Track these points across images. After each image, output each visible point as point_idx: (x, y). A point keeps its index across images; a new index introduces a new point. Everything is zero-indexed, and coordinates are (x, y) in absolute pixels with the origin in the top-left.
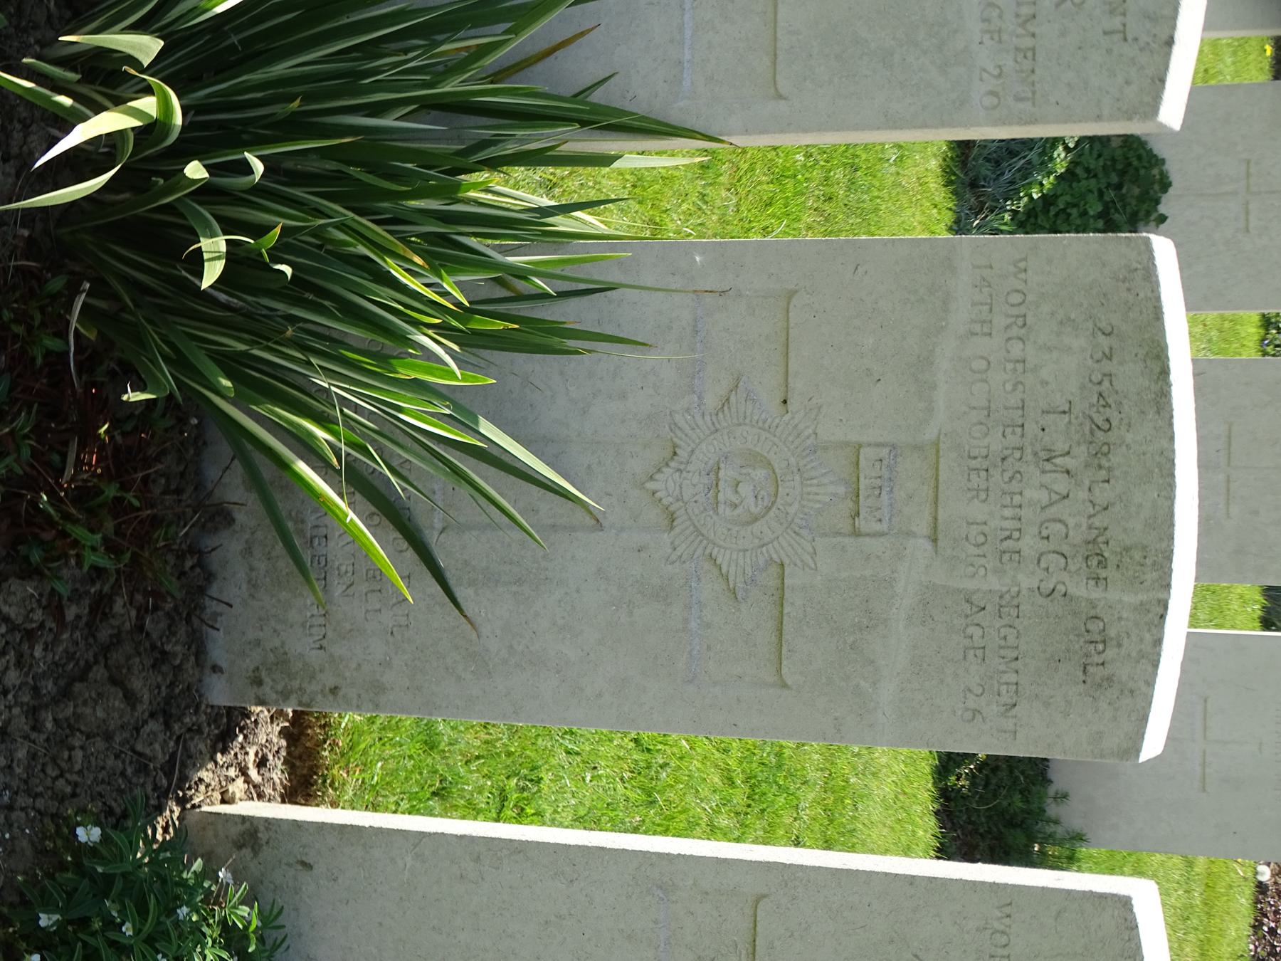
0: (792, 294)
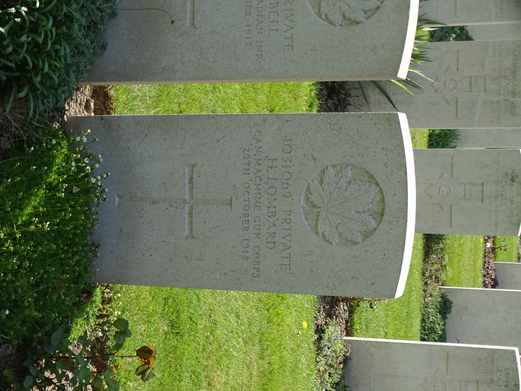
0: (459, 51)
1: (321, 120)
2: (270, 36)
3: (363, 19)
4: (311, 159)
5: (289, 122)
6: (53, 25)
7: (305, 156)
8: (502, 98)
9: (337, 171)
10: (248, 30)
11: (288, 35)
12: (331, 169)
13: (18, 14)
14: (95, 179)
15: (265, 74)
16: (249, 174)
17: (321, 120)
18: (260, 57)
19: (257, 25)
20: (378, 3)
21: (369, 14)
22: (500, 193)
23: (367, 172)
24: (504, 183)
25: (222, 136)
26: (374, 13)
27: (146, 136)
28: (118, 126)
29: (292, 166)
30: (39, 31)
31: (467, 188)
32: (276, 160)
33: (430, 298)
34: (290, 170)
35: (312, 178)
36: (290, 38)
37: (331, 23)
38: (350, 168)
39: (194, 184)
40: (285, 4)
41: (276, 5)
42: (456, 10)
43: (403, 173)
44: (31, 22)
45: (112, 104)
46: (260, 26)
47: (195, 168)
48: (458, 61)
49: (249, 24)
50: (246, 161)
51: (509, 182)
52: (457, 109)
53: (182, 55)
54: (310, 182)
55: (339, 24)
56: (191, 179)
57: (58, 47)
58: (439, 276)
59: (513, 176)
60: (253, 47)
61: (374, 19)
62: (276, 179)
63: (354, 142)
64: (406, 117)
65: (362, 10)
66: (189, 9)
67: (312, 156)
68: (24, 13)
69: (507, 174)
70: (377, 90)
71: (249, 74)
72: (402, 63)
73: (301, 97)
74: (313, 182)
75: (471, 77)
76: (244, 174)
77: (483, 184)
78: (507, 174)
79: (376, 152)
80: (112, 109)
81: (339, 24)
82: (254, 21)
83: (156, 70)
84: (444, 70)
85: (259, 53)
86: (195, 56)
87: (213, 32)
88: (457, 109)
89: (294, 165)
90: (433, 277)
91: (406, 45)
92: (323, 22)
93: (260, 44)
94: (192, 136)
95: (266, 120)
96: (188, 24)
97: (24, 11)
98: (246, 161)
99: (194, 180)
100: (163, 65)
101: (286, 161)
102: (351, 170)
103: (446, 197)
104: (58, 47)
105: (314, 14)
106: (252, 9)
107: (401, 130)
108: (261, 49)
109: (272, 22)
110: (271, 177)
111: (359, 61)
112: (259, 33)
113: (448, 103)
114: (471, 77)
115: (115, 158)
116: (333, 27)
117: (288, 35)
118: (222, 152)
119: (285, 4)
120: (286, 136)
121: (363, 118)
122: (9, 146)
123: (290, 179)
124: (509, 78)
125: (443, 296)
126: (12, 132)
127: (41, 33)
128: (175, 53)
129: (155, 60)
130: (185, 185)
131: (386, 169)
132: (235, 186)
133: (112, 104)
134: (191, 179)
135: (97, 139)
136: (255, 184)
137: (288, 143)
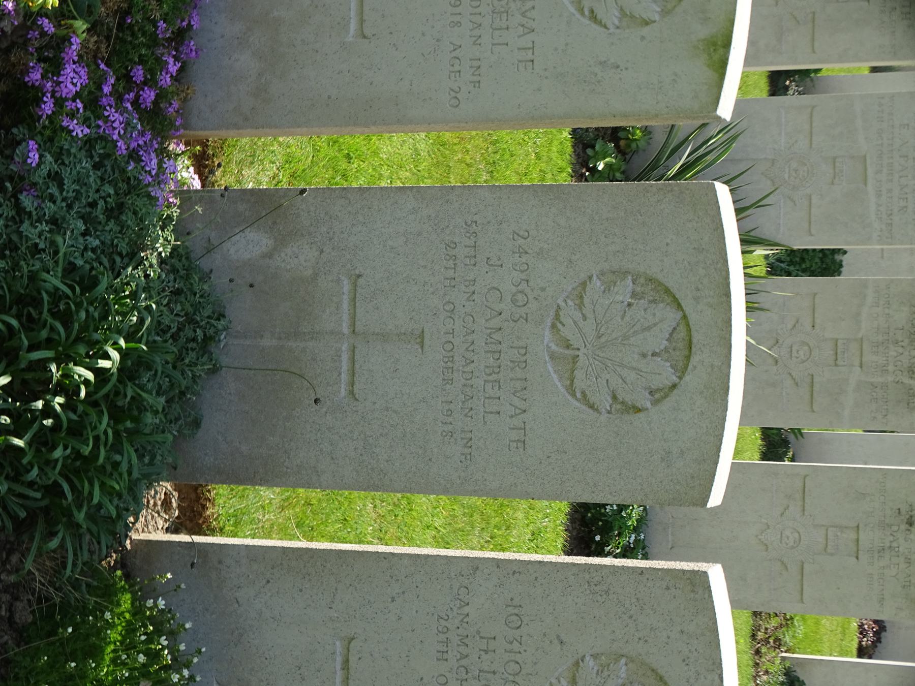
0: (815, 294)
1: (574, 575)
2: (485, 423)
3: (648, 405)
4: (556, 642)
5: (517, 575)
6: (108, 425)
7: (545, 635)
8: (890, 379)
9: (602, 665)
10: (448, 410)
11: (517, 422)
12: (590, 662)
13: (48, 411)
14: (178, 676)
15: (477, 488)
16: (447, 660)
17: (574, 575)
18: (469, 457)
19: (463, 402)
20: (674, 378)
21: (657, 396)
22: (888, 544)
23: (653, 670)
24: (895, 528)
25: (401, 591)
26: (666, 396)
27: (268, 582)
28: (220, 562)
29: (522, 651)
30: (85, 433)
31: (830, 533)
32: (494, 638)
33: (765, 677)
34: (518, 657)
35: (557, 674)
36: (521, 429)
37: (592, 407)
38: (623, 661)
39: (351, 671)
40: (512, 369)
41: (497, 370)
42: (810, 222)
43: (717, 677)
44: (69, 421)
45: (209, 491)
46: (469, 404)
47: (352, 644)
49: (450, 399)
50: (442, 637)
51: (904, 527)
52: (812, 395)
53: (332, 445)
54: (554, 681)
55: (606, 409)
56: (346, 662)
57: (118, 458)
58: (781, 637)
59: (911, 517)
60: (456, 440)
61: (667, 405)
62: (494, 673)
63: (631, 617)
64: (721, 570)
65: (645, 389)
66: (345, 366)
67: (558, 637)
68: (58, 408)
69: (899, 513)
71: (448, 486)
72: (714, 484)
73: (543, 155)
74: (559, 681)
75: (837, 340)
76: (438, 660)
77: (858, 527)
78: (899, 513)
79: (669, 637)
80: (210, 500)
81: (606, 409)
82: (458, 395)
83: (287, 468)
84: (790, 326)
85: (467, 451)
86: (355, 449)
87: (387, 409)
89: (525, 651)
90: (771, 641)
91: (722, 454)
92: (578, 404)
93: (469, 435)
94: (348, 588)
95: (477, 568)
96: (343, 392)
97: (59, 404)
98: (442, 637)
99: (351, 663)
100: (298, 461)
101: (511, 643)
102: (626, 664)
103: (792, 547)
104: (118, 458)
105: (563, 390)
106: (455, 374)
107: (712, 602)
108: (469, 444)
109: (489, 398)
110: (486, 668)
111: (641, 476)
112: (466, 415)
113: (797, 384)
114: (837, 340)
115: (214, 616)
116: (596, 414)
117: (517, 422)
118: (400, 618)
119: (512, 369)
120: (512, 599)
121: (647, 576)
122: (30, 619)
123: (517, 674)
124: (902, 344)
125: (788, 673)
126: (35, 590)
127: (88, 439)
128: (320, 441)
129: (286, 452)
130: (335, 673)
131: (686, 668)
132: (422, 679)
133: (209, 491)
134: (346, 662)
135: (183, 586)
136: (457, 679)
137: (516, 611)
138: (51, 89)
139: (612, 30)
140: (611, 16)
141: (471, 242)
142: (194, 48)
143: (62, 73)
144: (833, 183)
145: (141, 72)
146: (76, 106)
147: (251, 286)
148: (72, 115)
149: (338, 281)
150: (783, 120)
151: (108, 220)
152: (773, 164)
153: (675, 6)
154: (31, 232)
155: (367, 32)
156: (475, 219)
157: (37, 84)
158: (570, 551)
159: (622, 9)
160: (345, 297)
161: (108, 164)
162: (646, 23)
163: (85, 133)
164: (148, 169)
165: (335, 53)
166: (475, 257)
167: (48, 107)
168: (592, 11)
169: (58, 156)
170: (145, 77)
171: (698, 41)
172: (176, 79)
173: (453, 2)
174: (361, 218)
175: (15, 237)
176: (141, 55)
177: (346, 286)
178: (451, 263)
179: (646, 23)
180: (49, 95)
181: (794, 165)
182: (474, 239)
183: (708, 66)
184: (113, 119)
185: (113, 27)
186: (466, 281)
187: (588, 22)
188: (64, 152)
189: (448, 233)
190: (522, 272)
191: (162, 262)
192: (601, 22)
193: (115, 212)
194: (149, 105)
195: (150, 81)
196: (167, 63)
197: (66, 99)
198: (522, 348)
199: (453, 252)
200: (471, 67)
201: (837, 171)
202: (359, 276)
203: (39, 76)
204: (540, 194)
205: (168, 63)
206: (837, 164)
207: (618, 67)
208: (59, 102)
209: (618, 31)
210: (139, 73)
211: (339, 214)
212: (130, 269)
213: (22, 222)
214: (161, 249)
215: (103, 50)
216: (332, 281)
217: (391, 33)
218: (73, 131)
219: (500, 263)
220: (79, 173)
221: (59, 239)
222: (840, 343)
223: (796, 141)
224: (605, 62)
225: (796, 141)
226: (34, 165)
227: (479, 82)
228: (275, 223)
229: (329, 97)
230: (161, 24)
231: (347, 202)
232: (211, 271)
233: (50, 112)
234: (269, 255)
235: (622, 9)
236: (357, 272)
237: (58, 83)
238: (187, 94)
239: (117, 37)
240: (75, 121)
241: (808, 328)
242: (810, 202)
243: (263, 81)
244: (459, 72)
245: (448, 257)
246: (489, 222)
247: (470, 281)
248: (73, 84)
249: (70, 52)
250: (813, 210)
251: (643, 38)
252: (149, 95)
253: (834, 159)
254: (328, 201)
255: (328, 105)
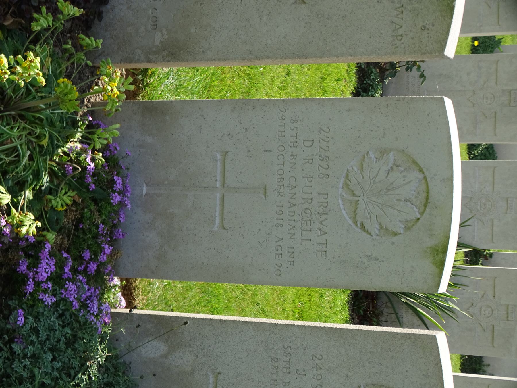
0: (495, 278)
36: (324, 244)
42: (492, 235)
48: (494, 288)
52: (493, 337)
70: (410, 311)
75: (508, 305)
88: (493, 337)
114: (508, 305)
138: (32, 277)
139: (374, 237)
140: (374, 229)
141: (287, 359)
142: (121, 234)
143: (39, 266)
144: (506, 213)
145: (88, 254)
146: (48, 287)
147: (154, 375)
148: (46, 291)
149: (207, 376)
150: (477, 174)
151: (67, 348)
152: (471, 199)
153: (413, 225)
154: (18, 367)
155: (226, 226)
156: (289, 345)
157: (24, 272)
158: (352, 321)
159: (380, 224)
160: (210, 385)
161: (67, 314)
162: (396, 234)
163: (53, 301)
164: (92, 312)
165: (206, 237)
166: (289, 368)
167: (30, 287)
168: (362, 224)
169: (37, 318)
170: (91, 256)
171: (427, 248)
172: (111, 255)
173: (278, 212)
174: (221, 339)
175: (9, 371)
176: (88, 245)
177: (211, 379)
178: (275, 371)
179: (396, 234)
180: (31, 280)
181: (484, 201)
182: (289, 357)
183: (433, 264)
184: (70, 289)
185: (72, 229)
186: (284, 382)
187: (360, 231)
188: (40, 314)
189: (273, 352)
190: (318, 380)
191: (100, 366)
192: (367, 231)
193: (71, 342)
194: (93, 272)
195: (94, 258)
196: (104, 248)
197: (42, 282)
198: (325, 194)
199: (276, 364)
200: (288, 252)
201: (509, 206)
202: (219, 374)
203: (25, 268)
204: (329, 333)
205: (105, 249)
206: (509, 202)
207: (378, 260)
208: (38, 284)
209: (378, 237)
210: (87, 255)
211: (208, 335)
212: (80, 374)
213: (14, 360)
214: (99, 359)
215: (66, 243)
216: (203, 375)
217: (240, 228)
218: (45, 302)
219: (304, 373)
220: (49, 324)
221: (36, 370)
222: (510, 307)
223: (485, 187)
224: (370, 256)
225: (485, 187)
226: (21, 325)
227: (293, 262)
228: (169, 337)
229: (203, 263)
230: (102, 226)
231: (213, 328)
232: (130, 363)
233: (31, 291)
234: (165, 356)
235: (380, 224)
236: (218, 371)
237: (37, 273)
238: (117, 256)
239: (74, 234)
240: (47, 295)
241: (491, 297)
242: (493, 224)
243: (163, 250)
244: (281, 254)
245: (273, 367)
246: (298, 348)
247: (286, 383)
248: (45, 272)
249: (44, 253)
250: (494, 228)
251: (393, 243)
252: (93, 267)
253: (507, 198)
254: (201, 327)
255: (202, 268)
